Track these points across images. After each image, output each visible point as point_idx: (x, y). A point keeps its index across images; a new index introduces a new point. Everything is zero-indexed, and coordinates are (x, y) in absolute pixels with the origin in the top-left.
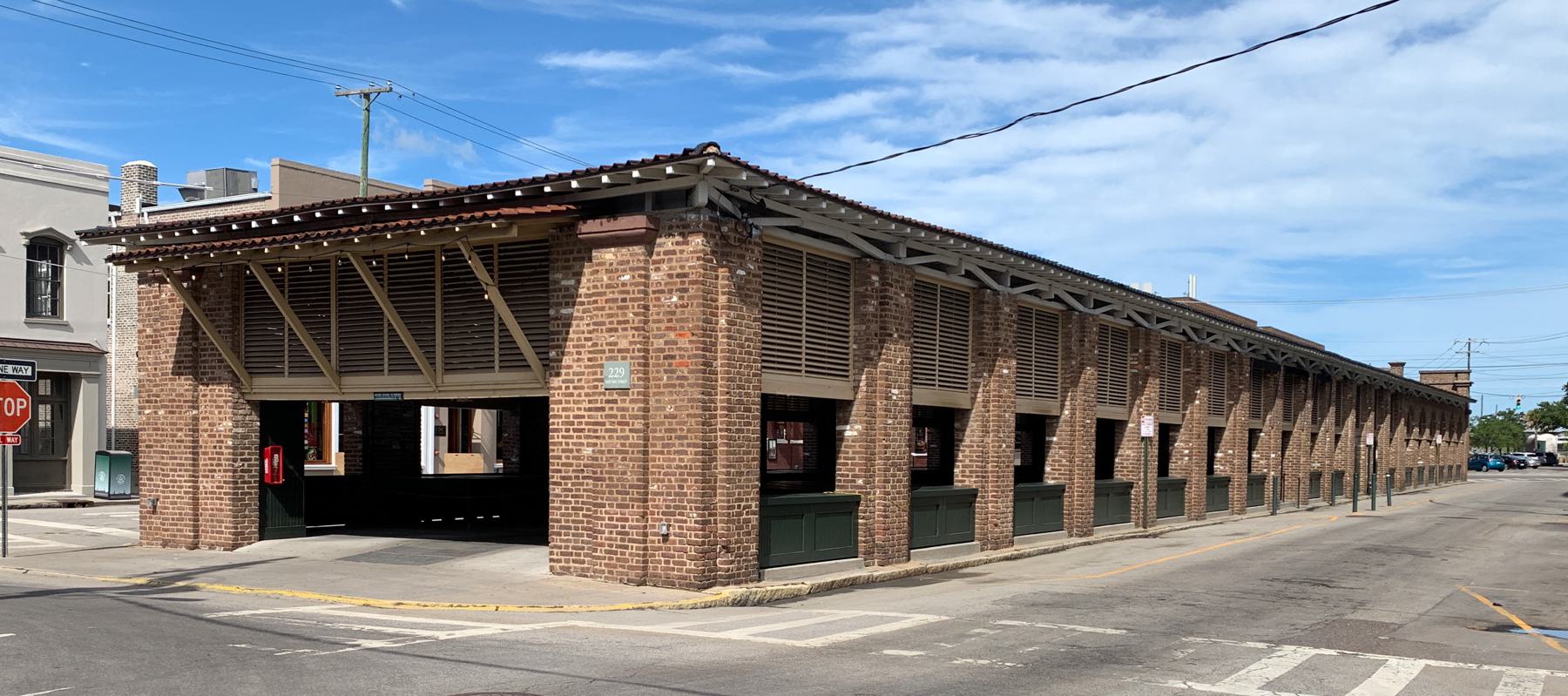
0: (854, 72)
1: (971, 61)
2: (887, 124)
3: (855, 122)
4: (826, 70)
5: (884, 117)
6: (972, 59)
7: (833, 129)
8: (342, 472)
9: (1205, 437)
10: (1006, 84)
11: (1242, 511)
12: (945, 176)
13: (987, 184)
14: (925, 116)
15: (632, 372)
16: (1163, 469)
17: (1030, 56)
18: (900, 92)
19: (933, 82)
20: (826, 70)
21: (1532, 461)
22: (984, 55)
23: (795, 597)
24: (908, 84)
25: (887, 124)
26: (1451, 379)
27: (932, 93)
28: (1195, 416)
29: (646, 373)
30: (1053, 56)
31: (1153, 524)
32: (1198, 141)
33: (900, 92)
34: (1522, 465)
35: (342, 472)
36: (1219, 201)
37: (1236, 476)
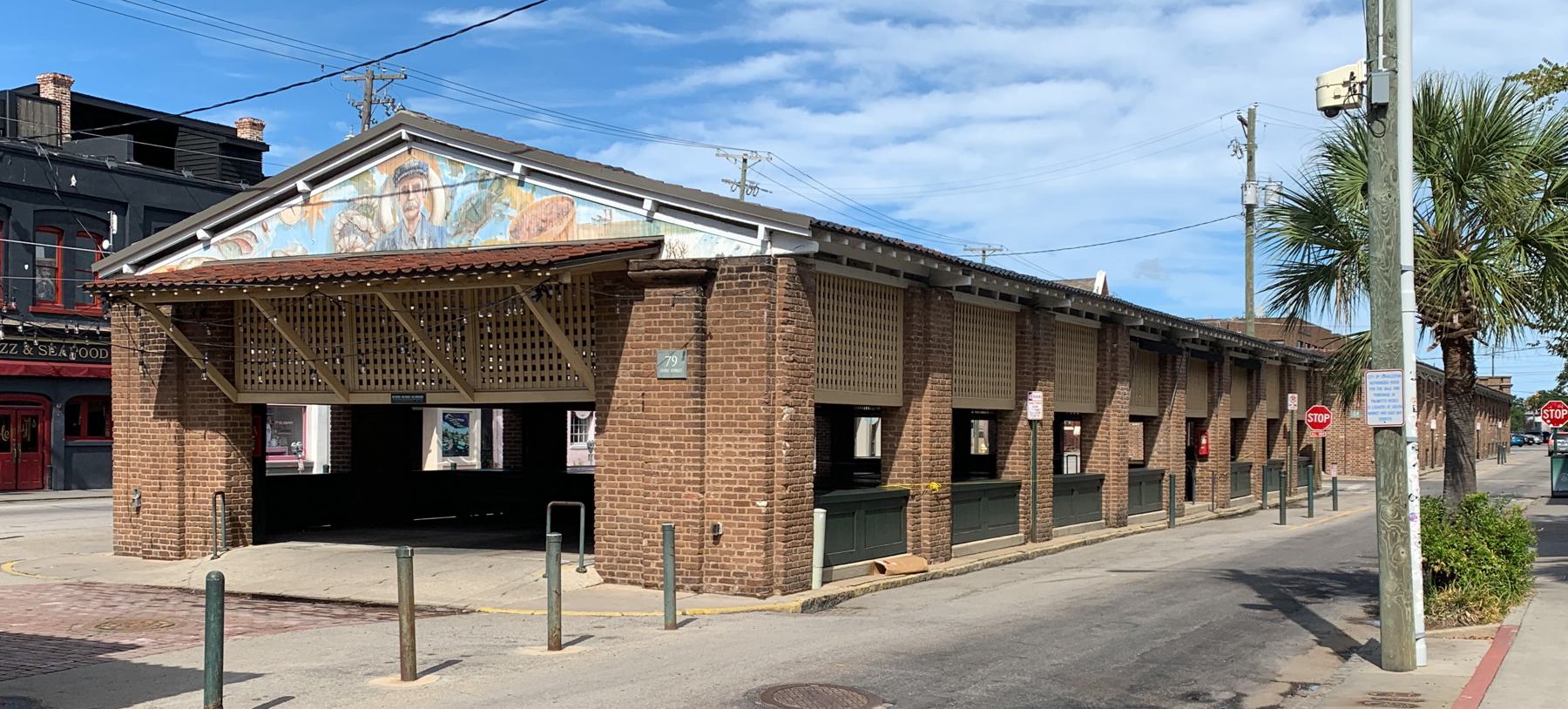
0: (759, 35)
1: (883, 25)
2: (801, 89)
3: (767, 86)
4: (732, 32)
5: (798, 80)
6: (883, 24)
7: (744, 93)
8: (478, 467)
9: (947, 424)
10: (919, 49)
11: (1121, 522)
12: (867, 143)
13: (913, 151)
14: (839, 81)
15: (689, 367)
16: (1235, 451)
17: (946, 22)
18: (812, 56)
19: (845, 46)
20: (732, 32)
21: (1537, 439)
22: (897, 20)
23: (969, 570)
24: (820, 47)
25: (801, 89)
26: (1498, 382)
27: (844, 58)
28: (1181, 406)
29: (703, 368)
30: (968, 23)
31: (1047, 537)
32: (1125, 111)
33: (812, 56)
34: (1529, 443)
35: (478, 467)
36: (1150, 171)
37: (1111, 476)
